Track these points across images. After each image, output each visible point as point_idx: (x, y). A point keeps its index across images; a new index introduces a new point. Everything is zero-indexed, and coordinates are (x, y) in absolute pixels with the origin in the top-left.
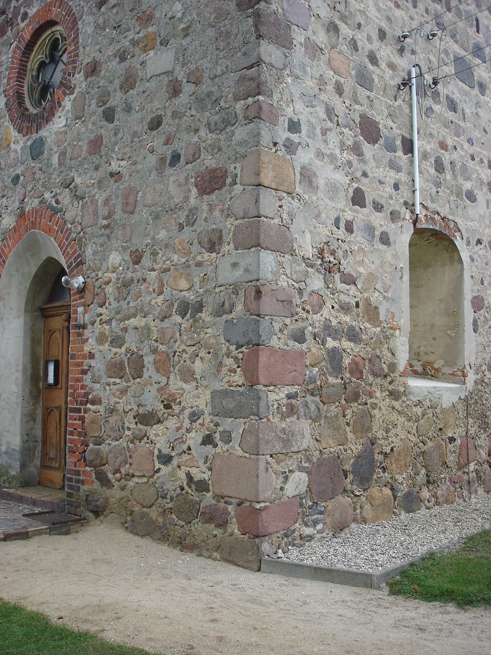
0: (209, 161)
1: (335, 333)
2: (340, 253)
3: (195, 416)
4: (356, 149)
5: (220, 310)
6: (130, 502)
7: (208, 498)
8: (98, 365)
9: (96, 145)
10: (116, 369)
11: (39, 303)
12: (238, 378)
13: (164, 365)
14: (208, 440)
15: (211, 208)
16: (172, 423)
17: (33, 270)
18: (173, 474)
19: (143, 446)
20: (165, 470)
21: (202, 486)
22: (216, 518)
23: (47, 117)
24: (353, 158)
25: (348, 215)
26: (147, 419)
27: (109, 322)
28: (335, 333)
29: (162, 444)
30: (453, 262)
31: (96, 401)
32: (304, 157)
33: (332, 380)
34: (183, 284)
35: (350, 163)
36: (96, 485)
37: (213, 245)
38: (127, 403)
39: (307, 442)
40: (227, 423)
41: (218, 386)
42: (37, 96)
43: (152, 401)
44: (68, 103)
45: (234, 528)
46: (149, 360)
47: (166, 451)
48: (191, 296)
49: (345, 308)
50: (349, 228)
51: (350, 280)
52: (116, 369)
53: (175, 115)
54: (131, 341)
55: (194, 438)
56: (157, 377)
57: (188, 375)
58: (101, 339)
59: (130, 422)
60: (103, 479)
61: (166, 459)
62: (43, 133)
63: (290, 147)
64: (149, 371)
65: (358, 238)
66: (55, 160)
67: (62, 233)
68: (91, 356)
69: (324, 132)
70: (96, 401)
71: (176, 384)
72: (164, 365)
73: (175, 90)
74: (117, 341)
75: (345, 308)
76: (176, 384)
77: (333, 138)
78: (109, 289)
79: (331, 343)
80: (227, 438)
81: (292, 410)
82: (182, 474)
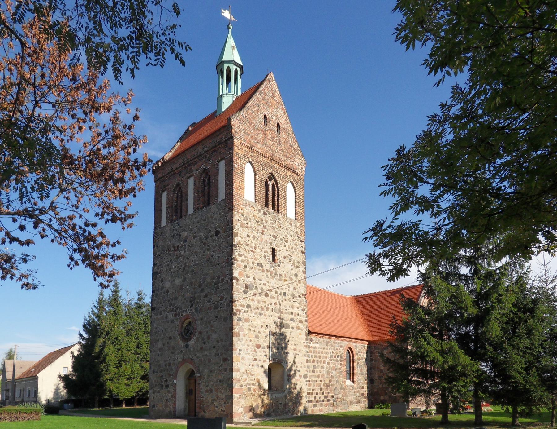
0: (225, 356)
1: (250, 384)
2: (250, 371)
3: (222, 399)
4: (255, 351)
6: (545, 344)
8: (203, 390)
9: (202, 348)
10: (207, 391)
11: (188, 376)
13: (217, 390)
16: (218, 401)
17: (187, 370)
18: (219, 409)
21: (224, 411)
23: (190, 339)
24: (254, 353)
25: (252, 363)
28: (250, 384)
32: (242, 355)
33: (248, 393)
34: (220, 377)
35: (253, 354)
39: (243, 403)
42: (186, 332)
44: (195, 338)
46: (214, 390)
49: (252, 380)
50: (253, 366)
51: (253, 375)
52: (207, 391)
53: (218, 346)
57: (221, 392)
62: (189, 343)
63: (239, 354)
65: (255, 367)
66: (192, 349)
69: (247, 349)
71: (219, 394)
72: (217, 390)
73: (218, 342)
75: (252, 380)
77: (249, 351)
79: (248, 386)
80: (228, 403)
81: (240, 398)
82: (220, 409)
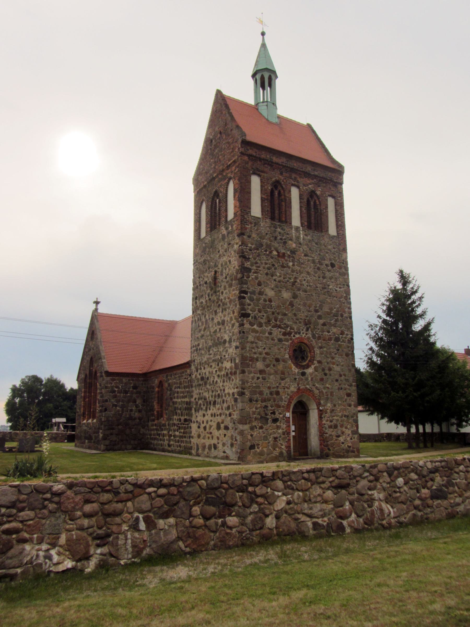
5: (352, 417)
7: (351, 448)
12: (355, 428)
13: (342, 426)
14: (351, 439)
15: (349, 400)
19: (338, 441)
20: (343, 445)
22: (353, 452)
26: (338, 436)
27: (329, 417)
29: (342, 440)
30: (463, 362)
31: (326, 433)
36: (328, 451)
37: (350, 405)
38: (334, 433)
40: (354, 436)
41: (352, 430)
43: (339, 432)
45: (356, 452)
46: (339, 425)
47: (343, 441)
48: (346, 414)
52: (330, 427)
54: (334, 422)
55: (348, 439)
56: (340, 428)
57: (346, 428)
58: (327, 421)
59: (335, 438)
60: (329, 449)
61: (343, 443)
64: (339, 427)
67: (195, 320)
68: (325, 424)
70: (326, 433)
71: (344, 429)
74: (331, 421)
76: (344, 429)
78: (328, 411)
80: (354, 438)
82: (346, 446)
